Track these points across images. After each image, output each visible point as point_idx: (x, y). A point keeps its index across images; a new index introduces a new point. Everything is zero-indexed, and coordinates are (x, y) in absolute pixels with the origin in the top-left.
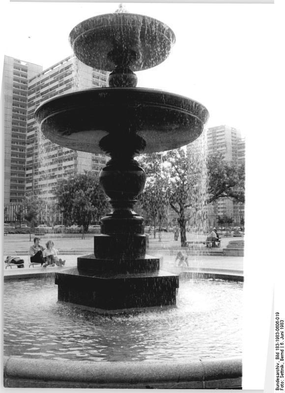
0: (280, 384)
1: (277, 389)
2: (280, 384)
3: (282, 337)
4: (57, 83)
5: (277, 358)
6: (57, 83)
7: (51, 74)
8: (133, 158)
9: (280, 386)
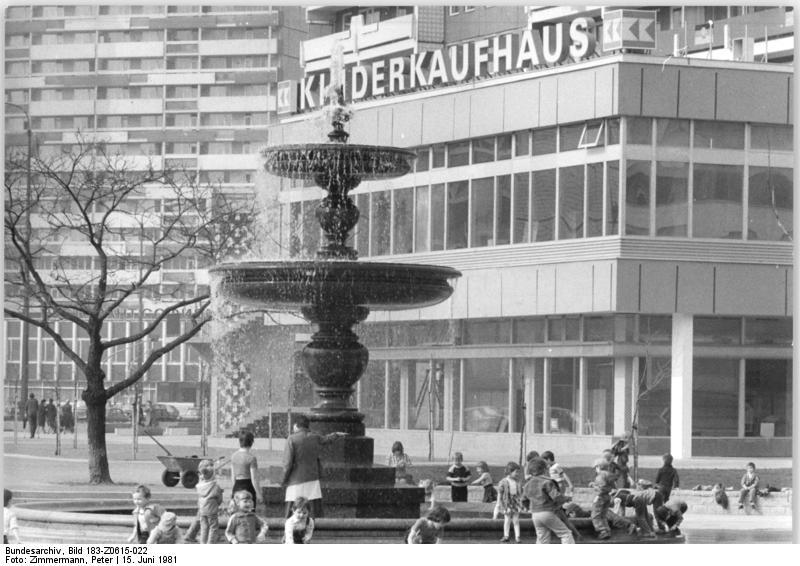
0: (19, 556)
2: (19, 556)
3: (142, 560)
9: (14, 556)
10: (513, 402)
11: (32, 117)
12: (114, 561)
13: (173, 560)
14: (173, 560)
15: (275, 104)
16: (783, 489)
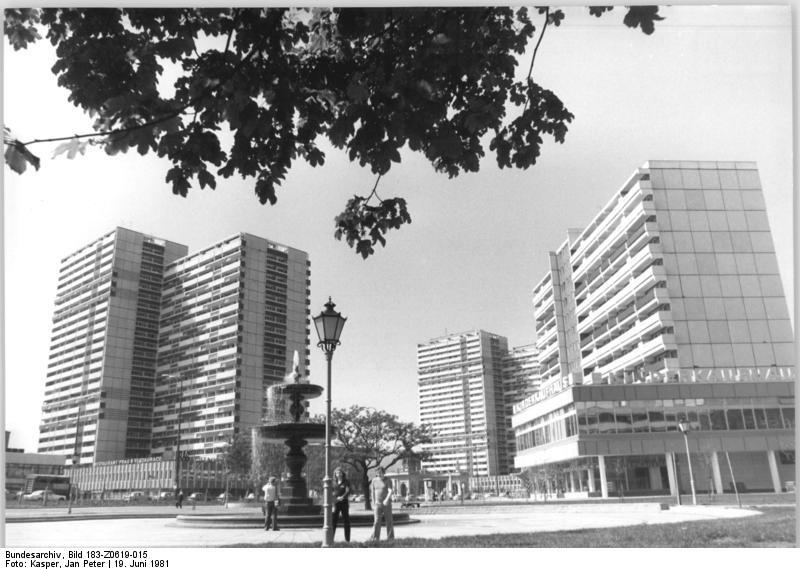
0: (19, 560)
1: (8, 554)
2: (19, 560)
3: (134, 564)
4: (207, 316)
5: (71, 554)
6: (207, 316)
7: (201, 261)
8: (182, 160)
9: (14, 560)
10: (652, 306)
11: (580, 453)
12: (106, 565)
13: (165, 564)
14: (165, 564)
15: (715, 192)
16: (671, 508)
